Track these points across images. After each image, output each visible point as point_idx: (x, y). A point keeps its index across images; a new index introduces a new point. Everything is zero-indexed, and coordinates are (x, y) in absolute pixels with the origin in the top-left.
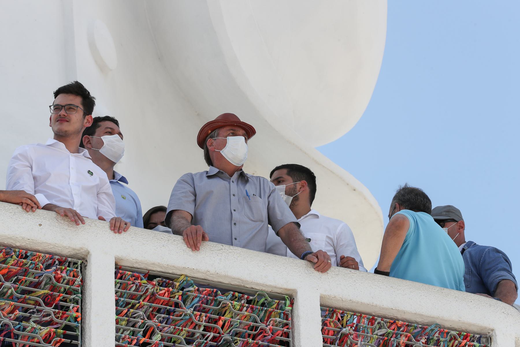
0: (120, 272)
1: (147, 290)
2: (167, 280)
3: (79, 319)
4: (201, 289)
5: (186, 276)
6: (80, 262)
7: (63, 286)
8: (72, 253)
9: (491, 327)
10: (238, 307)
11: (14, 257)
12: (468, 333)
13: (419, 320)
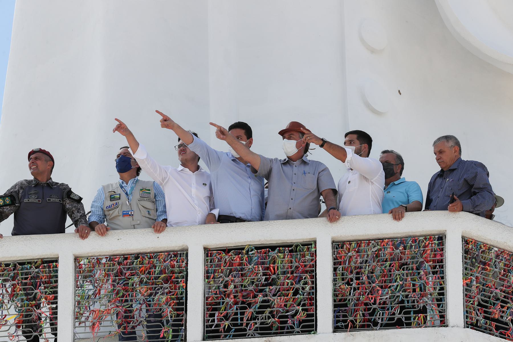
0: (466, 241)
1: (226, 259)
2: (239, 250)
3: (184, 287)
4: (259, 251)
5: (249, 245)
6: (185, 252)
7: (176, 269)
8: (180, 248)
9: (444, 229)
10: (282, 256)
11: (147, 259)
12: (430, 236)
13: (399, 235)
